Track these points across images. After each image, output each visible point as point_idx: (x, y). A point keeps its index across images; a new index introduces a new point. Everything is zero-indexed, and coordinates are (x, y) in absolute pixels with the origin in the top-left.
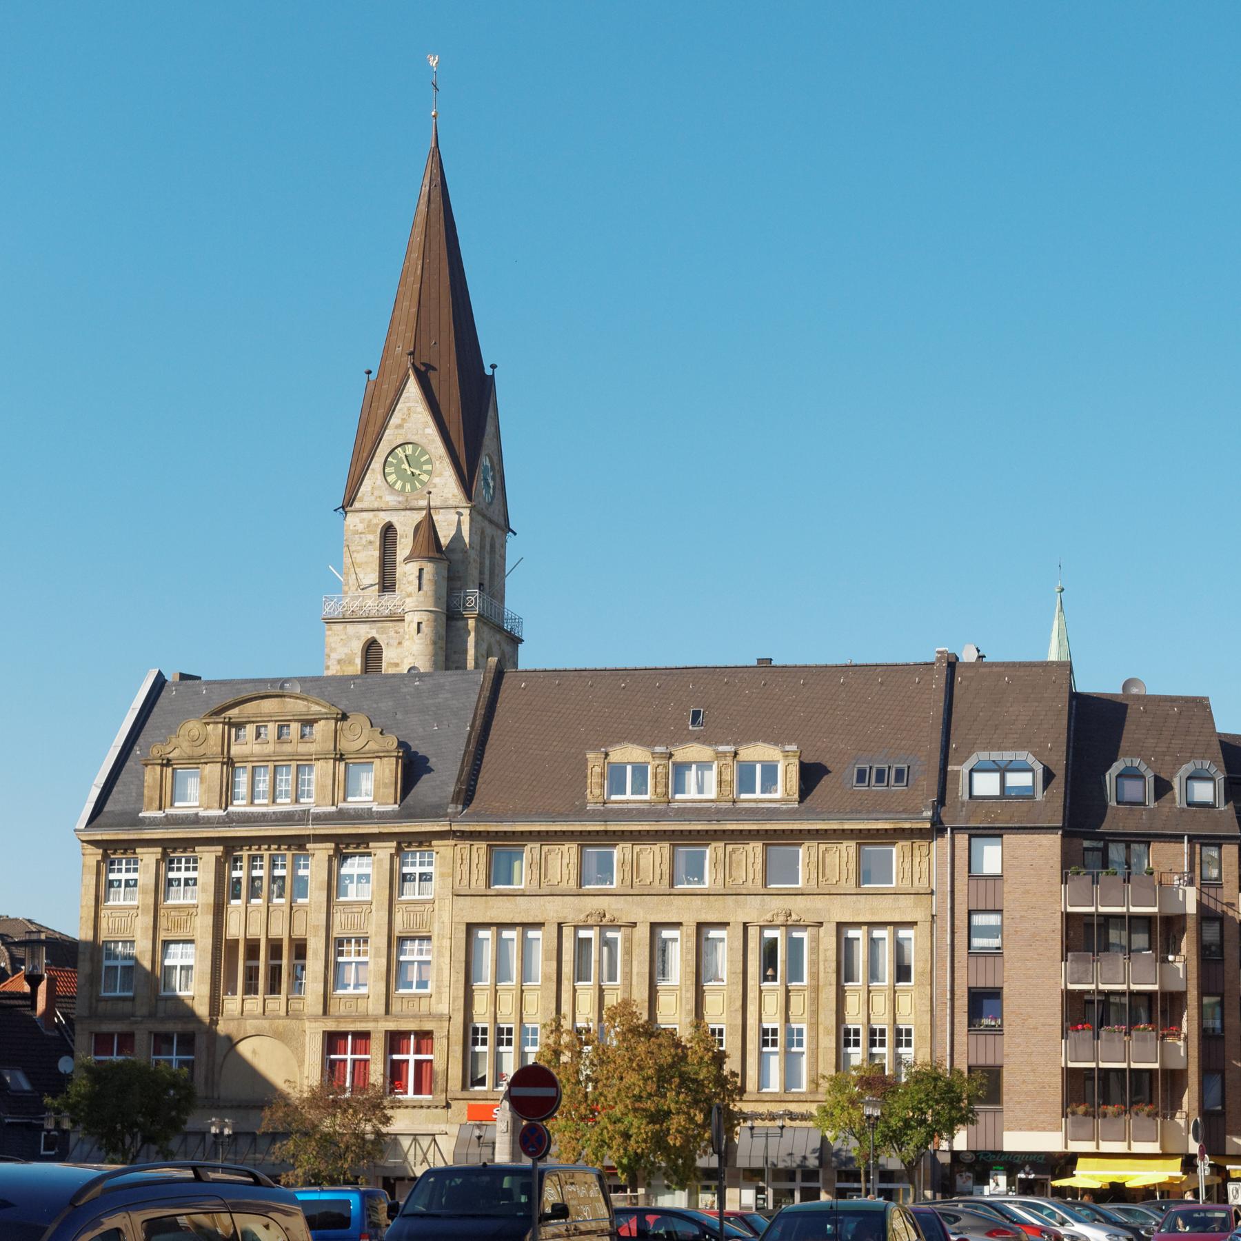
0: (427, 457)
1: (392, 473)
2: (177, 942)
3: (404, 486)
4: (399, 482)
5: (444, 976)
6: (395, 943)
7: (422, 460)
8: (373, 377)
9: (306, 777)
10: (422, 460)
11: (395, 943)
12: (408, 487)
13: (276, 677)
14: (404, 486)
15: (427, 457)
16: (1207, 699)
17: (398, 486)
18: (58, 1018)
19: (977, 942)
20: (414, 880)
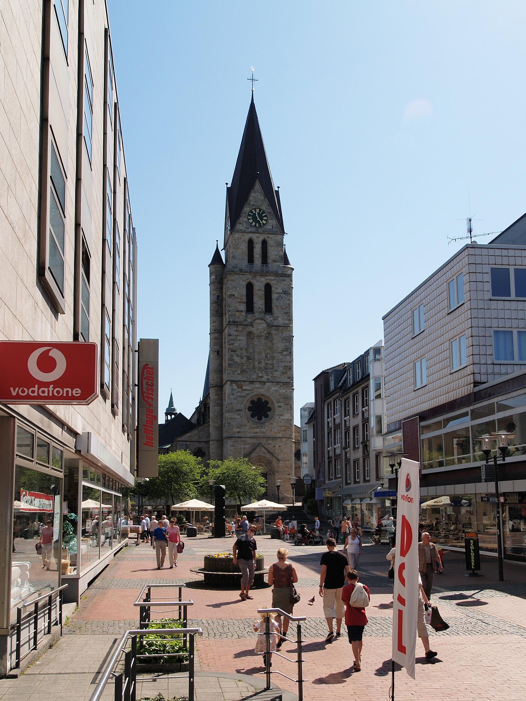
0: (265, 214)
1: (251, 219)
2: (168, 569)
3: (256, 224)
4: (254, 222)
5: (102, 670)
6: (59, 570)
7: (263, 215)
8: (229, 186)
9: (456, 457)
10: (263, 215)
11: (59, 570)
12: (257, 225)
13: (37, 226)
14: (256, 224)
15: (265, 214)
16: (405, 557)
17: (254, 224)
18: (166, 656)
19: (122, 652)
20: (486, 463)
